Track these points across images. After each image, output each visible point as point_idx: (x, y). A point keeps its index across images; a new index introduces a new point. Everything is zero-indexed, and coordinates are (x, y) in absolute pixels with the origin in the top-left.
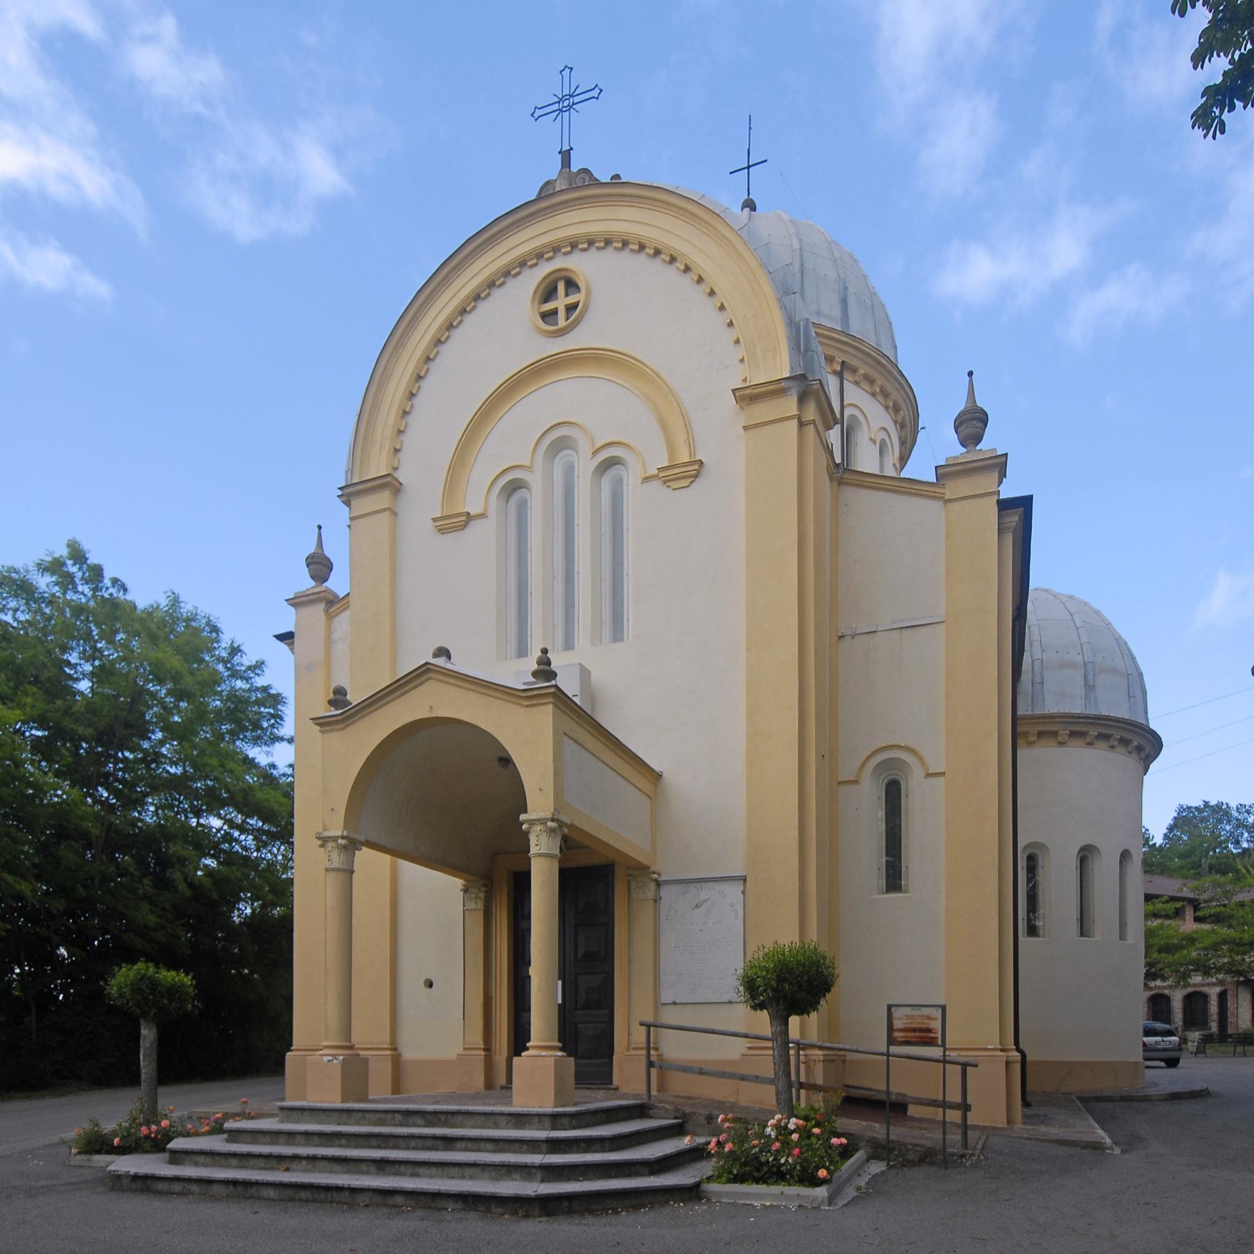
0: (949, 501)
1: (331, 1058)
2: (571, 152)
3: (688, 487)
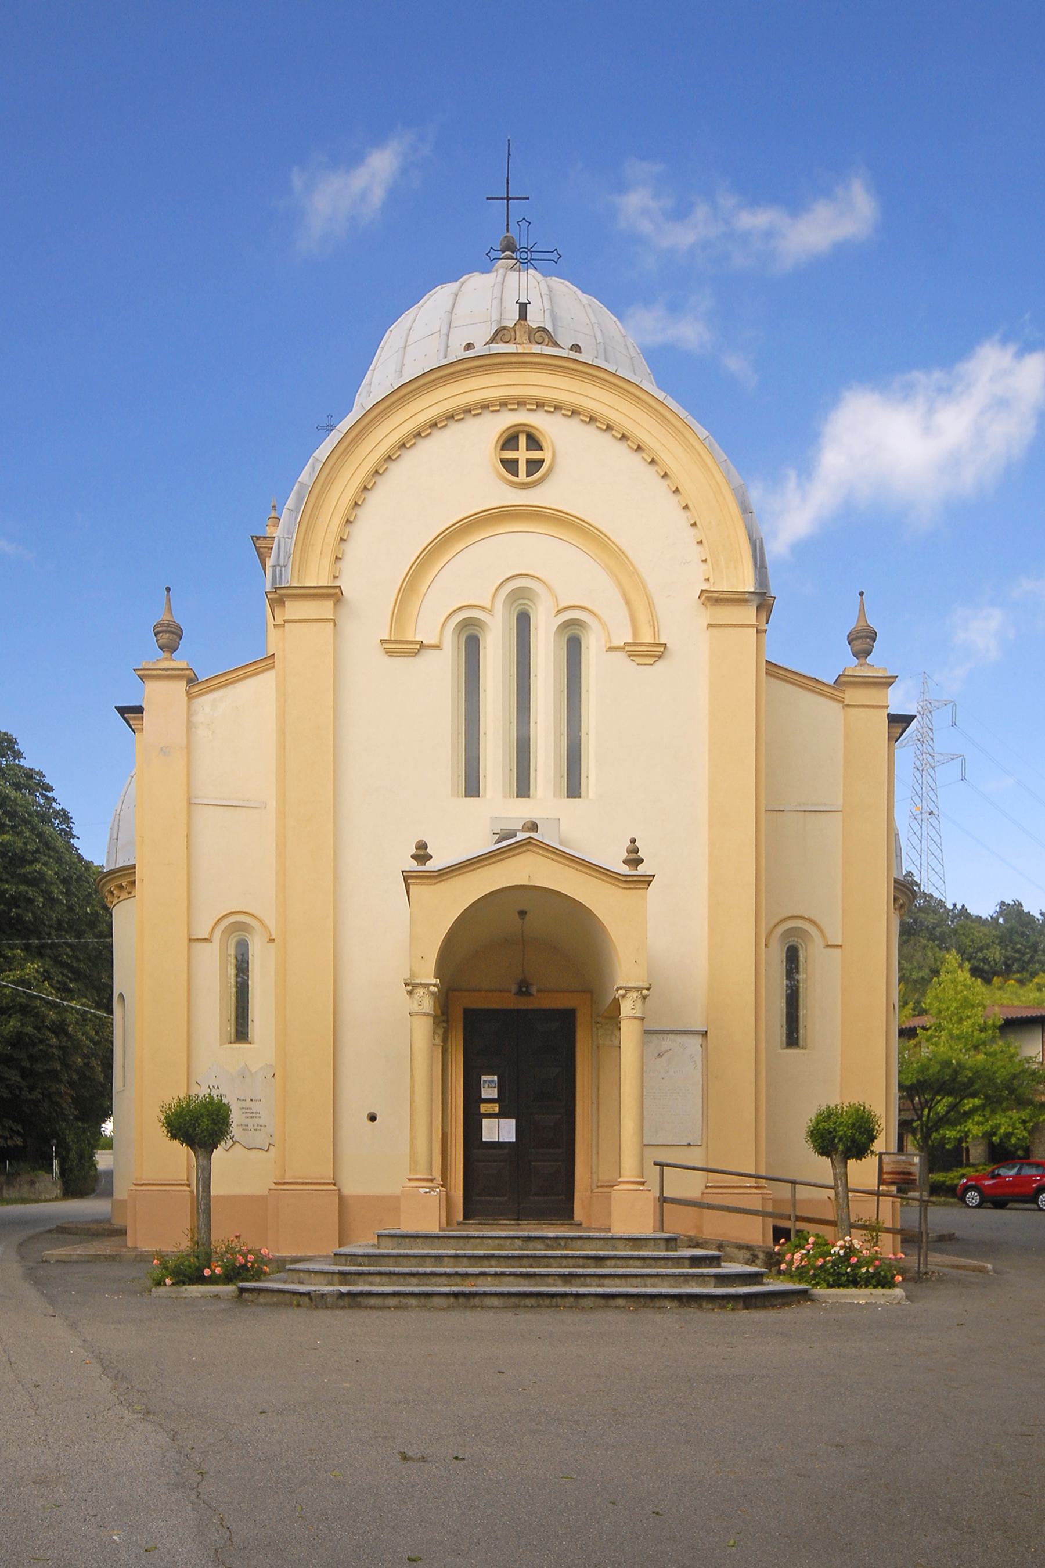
0: (848, 706)
1: (428, 1190)
2: (528, 305)
3: (652, 664)
